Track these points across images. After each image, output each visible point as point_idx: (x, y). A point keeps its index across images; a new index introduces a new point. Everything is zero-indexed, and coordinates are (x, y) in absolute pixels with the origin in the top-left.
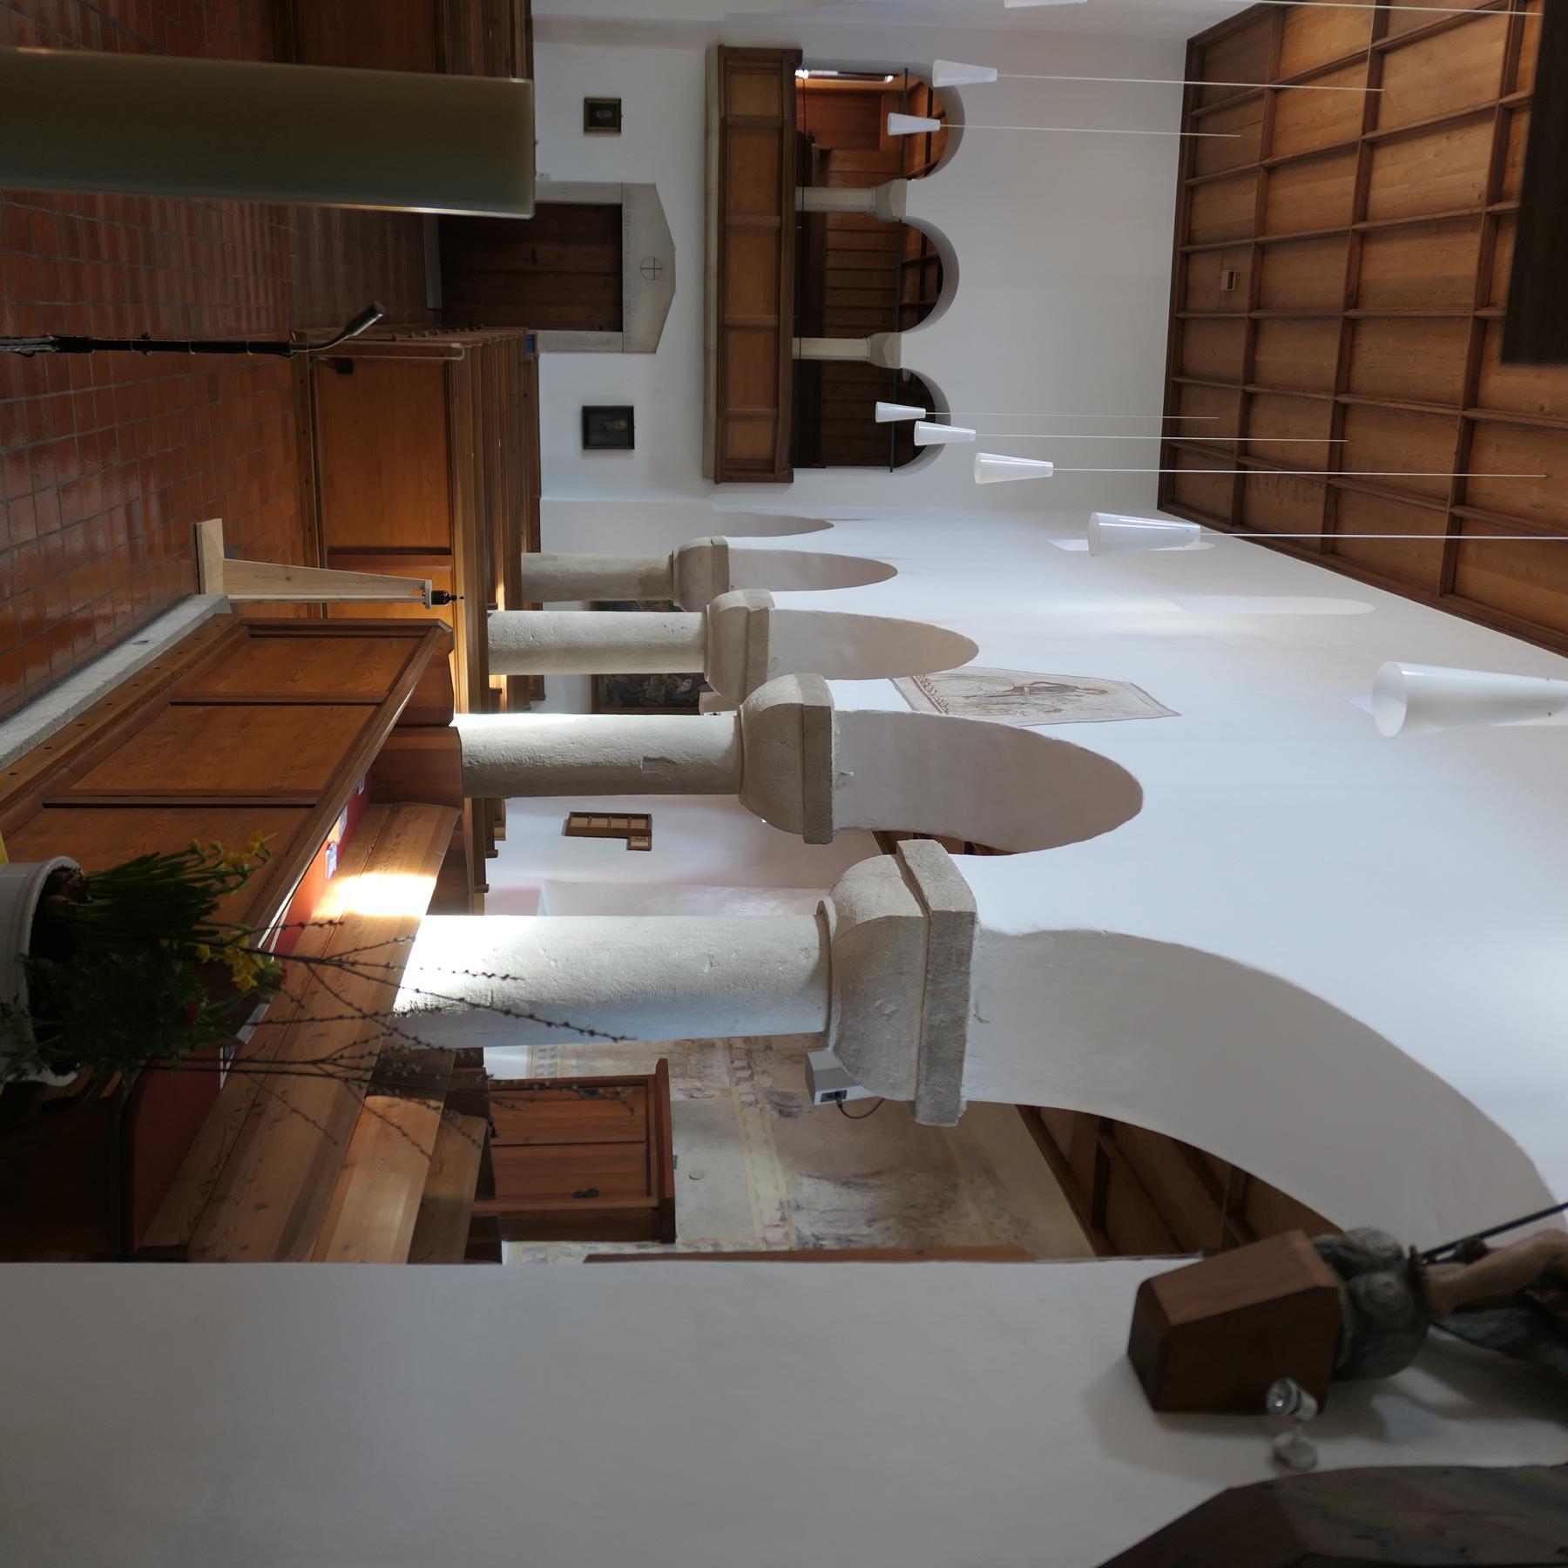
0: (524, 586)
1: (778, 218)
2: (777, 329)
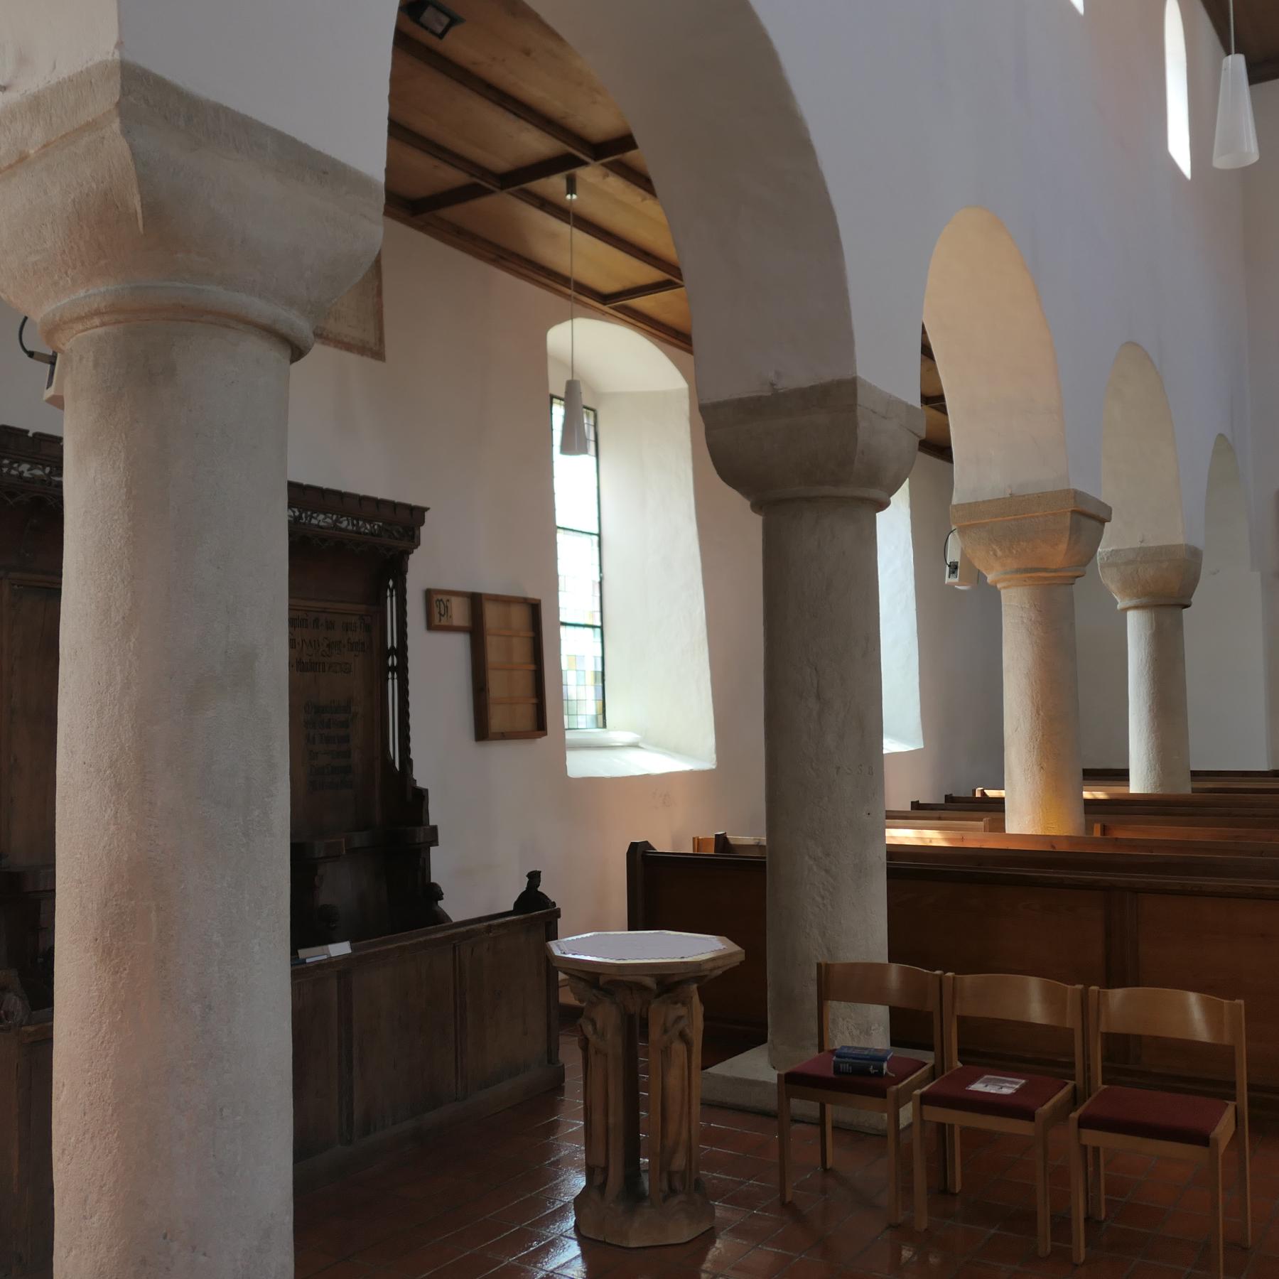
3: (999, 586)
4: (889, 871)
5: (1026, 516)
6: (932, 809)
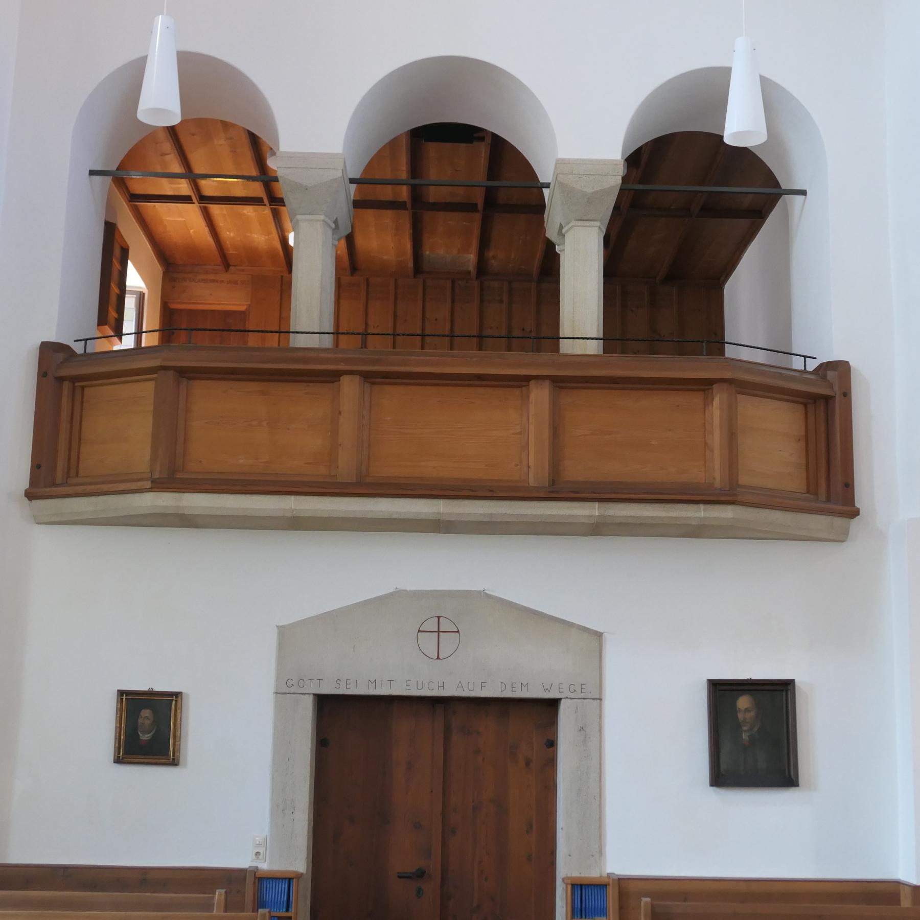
1: (345, 379)
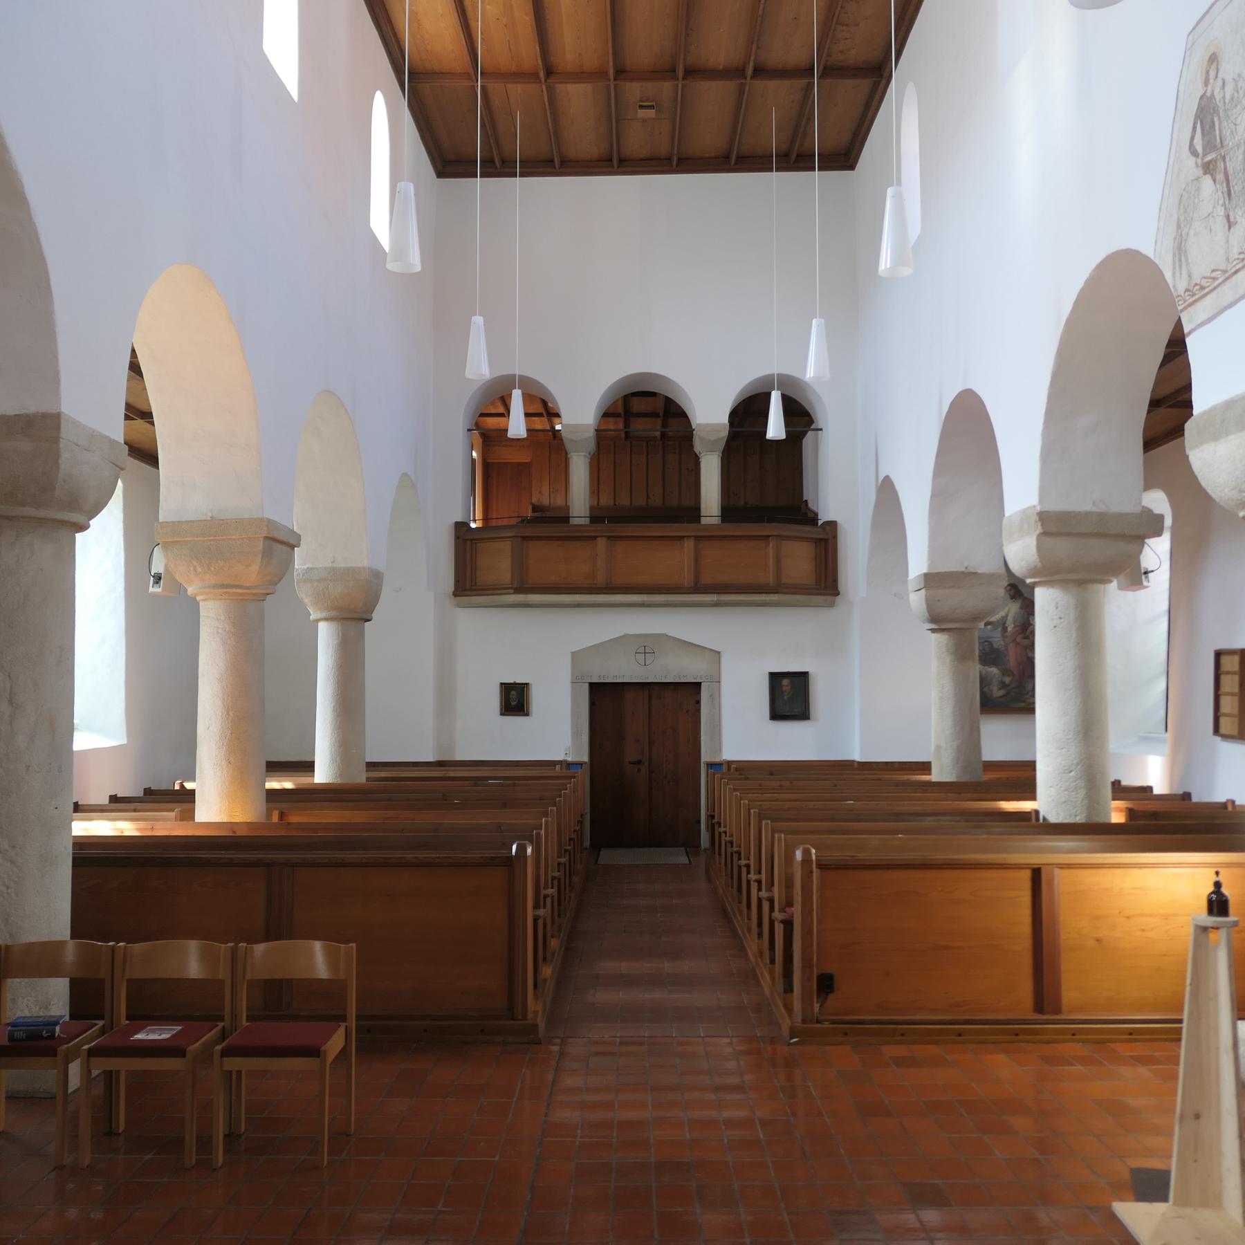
0: (966, 778)
1: (599, 539)
2: (696, 537)
3: (198, 598)
4: (74, 859)
5: (224, 537)
6: (130, 802)
